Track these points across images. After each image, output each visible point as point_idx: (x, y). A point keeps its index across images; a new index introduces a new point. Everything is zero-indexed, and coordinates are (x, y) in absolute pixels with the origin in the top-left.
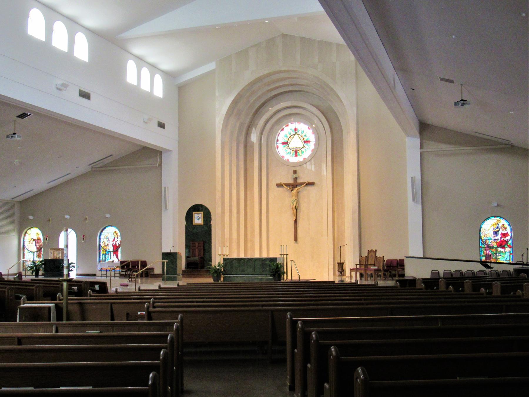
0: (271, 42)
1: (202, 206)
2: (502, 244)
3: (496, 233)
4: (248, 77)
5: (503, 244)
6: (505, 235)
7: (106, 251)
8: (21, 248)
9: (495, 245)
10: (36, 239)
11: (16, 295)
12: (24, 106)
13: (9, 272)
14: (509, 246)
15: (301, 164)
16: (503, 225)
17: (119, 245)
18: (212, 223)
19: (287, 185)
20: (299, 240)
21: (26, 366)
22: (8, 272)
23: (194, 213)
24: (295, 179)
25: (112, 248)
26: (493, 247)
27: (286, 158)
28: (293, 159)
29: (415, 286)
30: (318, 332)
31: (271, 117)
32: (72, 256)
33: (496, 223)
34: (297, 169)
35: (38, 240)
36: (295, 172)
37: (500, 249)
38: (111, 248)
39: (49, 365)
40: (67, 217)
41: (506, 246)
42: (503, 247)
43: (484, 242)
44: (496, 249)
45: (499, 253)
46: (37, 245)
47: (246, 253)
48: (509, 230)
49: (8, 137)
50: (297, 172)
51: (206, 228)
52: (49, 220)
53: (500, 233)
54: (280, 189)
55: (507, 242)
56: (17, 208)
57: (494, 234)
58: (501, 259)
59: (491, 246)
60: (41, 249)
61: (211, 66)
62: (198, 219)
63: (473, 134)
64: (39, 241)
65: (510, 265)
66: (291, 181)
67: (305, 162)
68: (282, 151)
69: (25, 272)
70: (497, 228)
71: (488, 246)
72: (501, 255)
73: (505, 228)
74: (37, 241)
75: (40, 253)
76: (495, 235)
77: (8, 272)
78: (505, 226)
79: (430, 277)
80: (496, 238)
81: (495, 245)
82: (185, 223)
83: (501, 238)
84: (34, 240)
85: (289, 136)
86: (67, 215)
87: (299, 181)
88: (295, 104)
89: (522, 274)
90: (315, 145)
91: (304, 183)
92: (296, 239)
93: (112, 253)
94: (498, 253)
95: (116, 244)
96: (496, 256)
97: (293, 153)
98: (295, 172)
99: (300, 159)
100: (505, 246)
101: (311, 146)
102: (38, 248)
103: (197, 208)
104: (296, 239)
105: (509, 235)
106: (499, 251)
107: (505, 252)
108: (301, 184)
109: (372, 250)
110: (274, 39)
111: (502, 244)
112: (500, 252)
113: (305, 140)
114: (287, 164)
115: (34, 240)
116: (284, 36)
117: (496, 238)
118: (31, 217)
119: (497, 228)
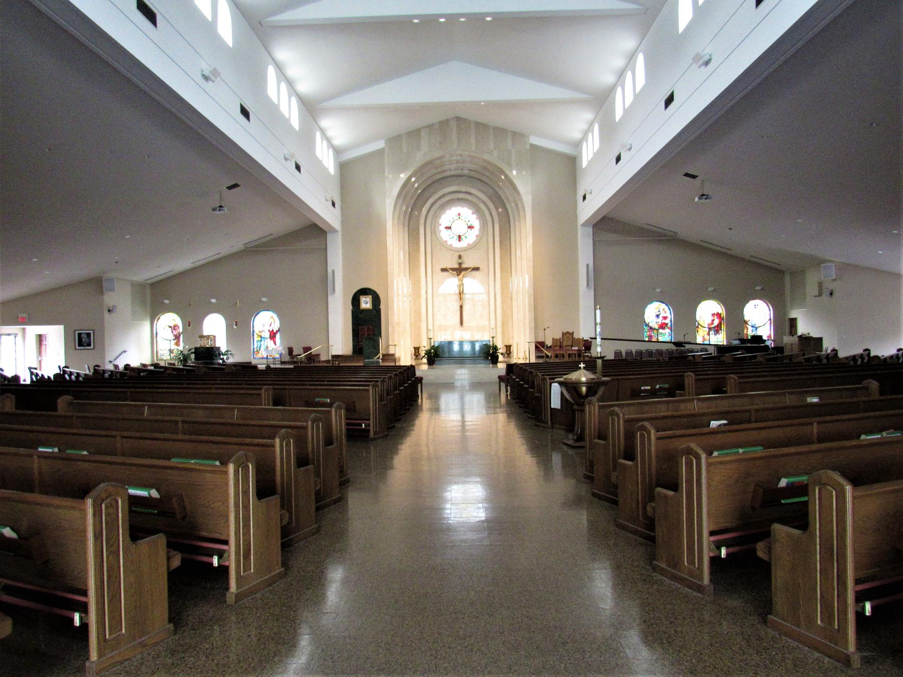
0: (444, 125)
1: (370, 290)
2: (663, 326)
3: (658, 316)
4: (420, 158)
6: (665, 318)
7: (261, 337)
8: (154, 336)
9: (657, 327)
10: (173, 326)
14: (668, 328)
15: (465, 250)
17: (277, 331)
18: (381, 307)
19: (453, 269)
20: (464, 324)
23: (361, 297)
24: (460, 264)
25: (269, 334)
26: (655, 329)
27: (449, 243)
28: (456, 244)
29: (55, 409)
30: (362, 426)
31: (435, 202)
34: (462, 254)
35: (175, 326)
36: (460, 257)
37: (661, 331)
38: (267, 335)
40: (213, 301)
42: (664, 329)
43: (647, 325)
44: (658, 330)
46: (174, 331)
48: (668, 314)
49: (214, 210)
50: (462, 258)
51: (374, 312)
52: (190, 305)
53: (661, 316)
54: (445, 273)
56: (148, 291)
58: (661, 339)
60: (180, 336)
61: (380, 144)
62: (366, 303)
63: (646, 226)
64: (176, 328)
66: (457, 266)
67: (470, 248)
68: (444, 235)
71: (651, 328)
74: (174, 328)
75: (179, 341)
79: (613, 358)
80: (658, 320)
81: (657, 327)
82: (351, 307)
84: (170, 327)
85: (452, 220)
86: (166, 299)
87: (464, 266)
88: (463, 189)
89: (59, 401)
90: (480, 230)
91: (470, 268)
92: (461, 323)
93: (269, 339)
95: (273, 330)
97: (456, 237)
98: (460, 257)
99: (463, 244)
101: (476, 231)
102: (175, 336)
103: (364, 292)
104: (461, 323)
108: (467, 269)
109: (567, 333)
110: (447, 121)
111: (663, 326)
112: (661, 333)
113: (469, 225)
114: (450, 249)
115: (170, 327)
116: (458, 119)
117: (658, 320)
118: (167, 302)
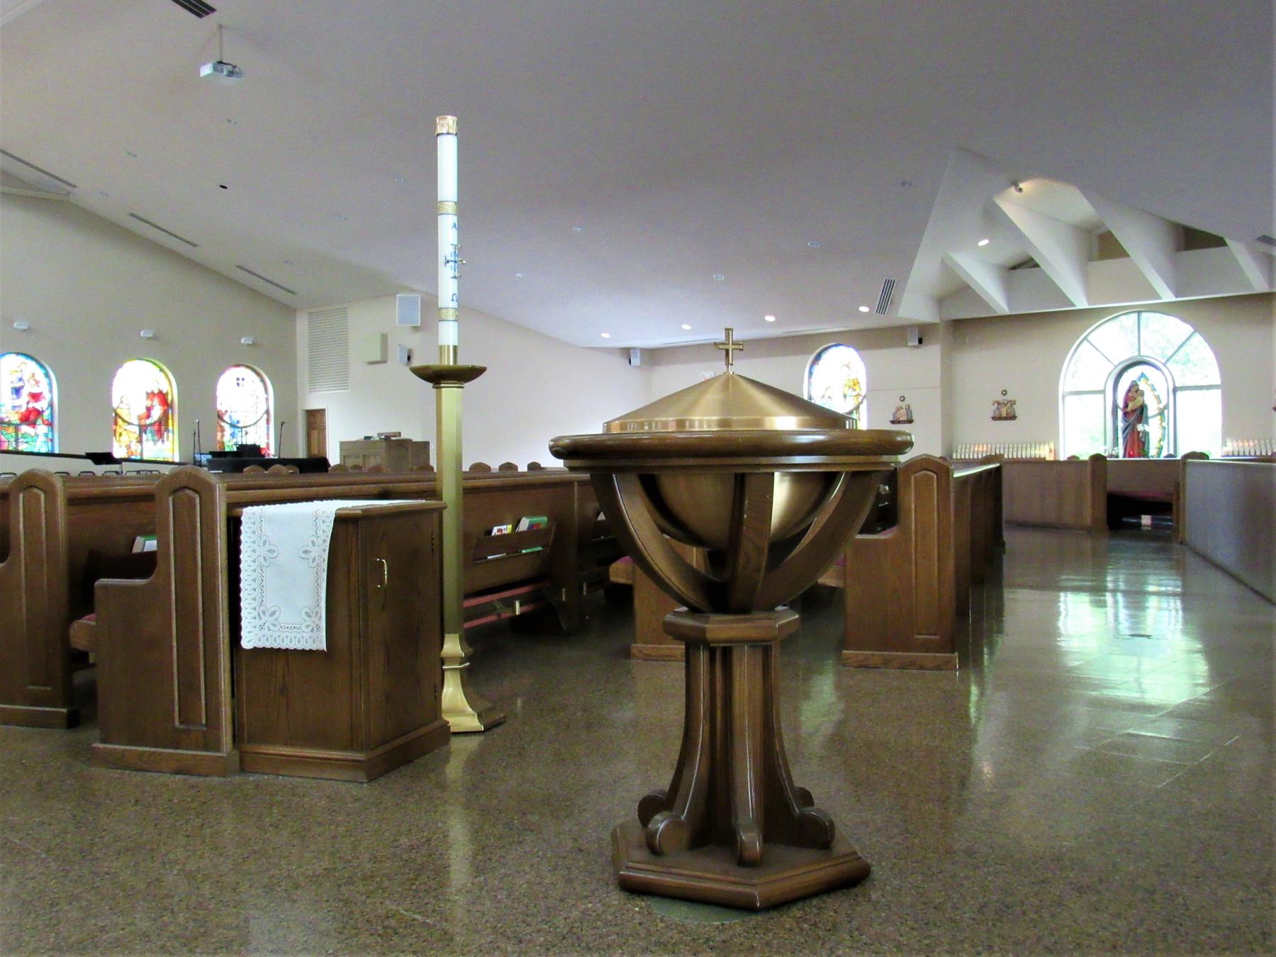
5: (32, 417)
6: (36, 397)
9: (15, 419)
11: (467, 608)
12: (358, 579)
13: (1088, 344)
16: (34, 375)
21: (412, 509)
22: (1089, 342)
26: (9, 424)
32: (636, 645)
33: (18, 369)
37: (25, 429)
39: (401, 510)
41: (39, 421)
42: (33, 424)
45: (25, 438)
47: (455, 361)
55: (39, 413)
57: (12, 393)
59: (6, 420)
65: (52, 458)
69: (458, 359)
70: (21, 379)
72: (27, 443)
73: (37, 383)
76: (15, 396)
77: (1089, 342)
78: (37, 377)
83: (28, 403)
94: (22, 438)
96: (17, 444)
100: (36, 422)
105: (45, 398)
106: (23, 432)
107: (37, 435)
111: (30, 417)
117: (17, 402)
119: (21, 379)
